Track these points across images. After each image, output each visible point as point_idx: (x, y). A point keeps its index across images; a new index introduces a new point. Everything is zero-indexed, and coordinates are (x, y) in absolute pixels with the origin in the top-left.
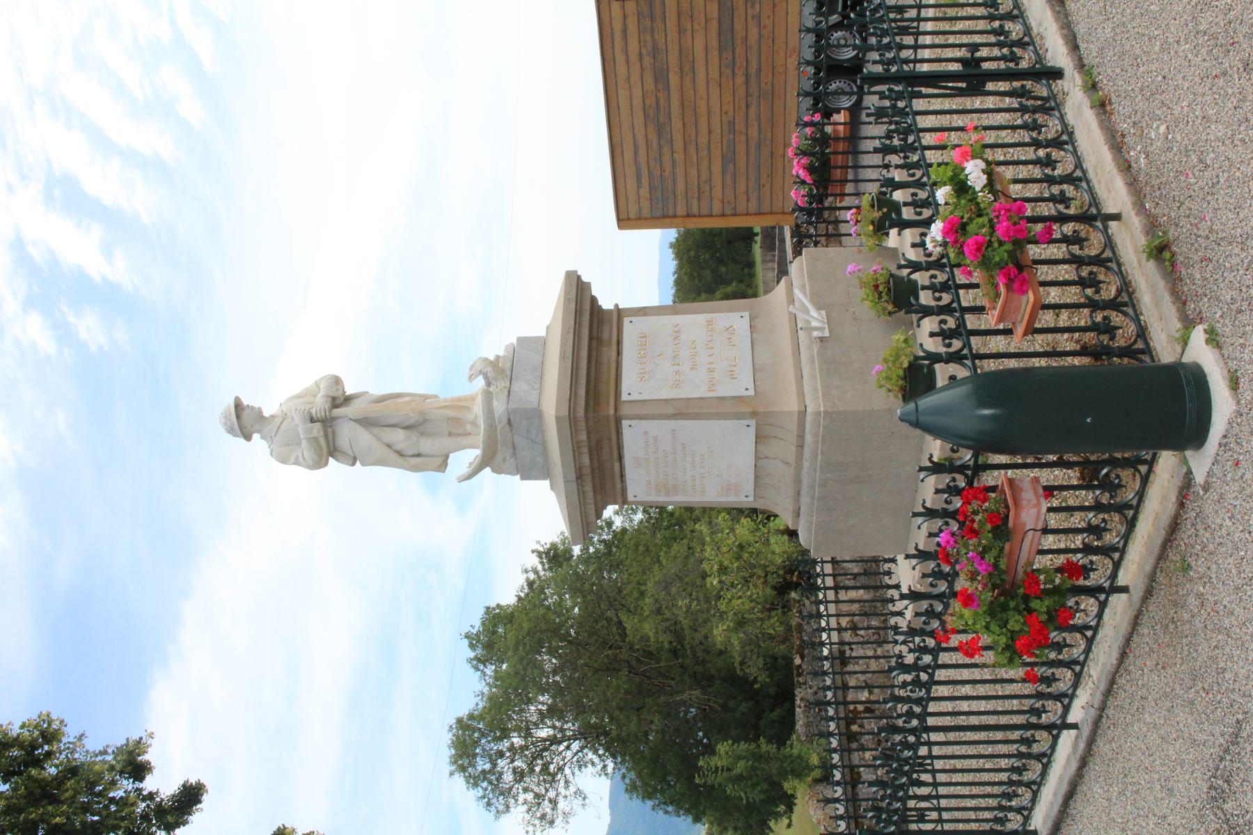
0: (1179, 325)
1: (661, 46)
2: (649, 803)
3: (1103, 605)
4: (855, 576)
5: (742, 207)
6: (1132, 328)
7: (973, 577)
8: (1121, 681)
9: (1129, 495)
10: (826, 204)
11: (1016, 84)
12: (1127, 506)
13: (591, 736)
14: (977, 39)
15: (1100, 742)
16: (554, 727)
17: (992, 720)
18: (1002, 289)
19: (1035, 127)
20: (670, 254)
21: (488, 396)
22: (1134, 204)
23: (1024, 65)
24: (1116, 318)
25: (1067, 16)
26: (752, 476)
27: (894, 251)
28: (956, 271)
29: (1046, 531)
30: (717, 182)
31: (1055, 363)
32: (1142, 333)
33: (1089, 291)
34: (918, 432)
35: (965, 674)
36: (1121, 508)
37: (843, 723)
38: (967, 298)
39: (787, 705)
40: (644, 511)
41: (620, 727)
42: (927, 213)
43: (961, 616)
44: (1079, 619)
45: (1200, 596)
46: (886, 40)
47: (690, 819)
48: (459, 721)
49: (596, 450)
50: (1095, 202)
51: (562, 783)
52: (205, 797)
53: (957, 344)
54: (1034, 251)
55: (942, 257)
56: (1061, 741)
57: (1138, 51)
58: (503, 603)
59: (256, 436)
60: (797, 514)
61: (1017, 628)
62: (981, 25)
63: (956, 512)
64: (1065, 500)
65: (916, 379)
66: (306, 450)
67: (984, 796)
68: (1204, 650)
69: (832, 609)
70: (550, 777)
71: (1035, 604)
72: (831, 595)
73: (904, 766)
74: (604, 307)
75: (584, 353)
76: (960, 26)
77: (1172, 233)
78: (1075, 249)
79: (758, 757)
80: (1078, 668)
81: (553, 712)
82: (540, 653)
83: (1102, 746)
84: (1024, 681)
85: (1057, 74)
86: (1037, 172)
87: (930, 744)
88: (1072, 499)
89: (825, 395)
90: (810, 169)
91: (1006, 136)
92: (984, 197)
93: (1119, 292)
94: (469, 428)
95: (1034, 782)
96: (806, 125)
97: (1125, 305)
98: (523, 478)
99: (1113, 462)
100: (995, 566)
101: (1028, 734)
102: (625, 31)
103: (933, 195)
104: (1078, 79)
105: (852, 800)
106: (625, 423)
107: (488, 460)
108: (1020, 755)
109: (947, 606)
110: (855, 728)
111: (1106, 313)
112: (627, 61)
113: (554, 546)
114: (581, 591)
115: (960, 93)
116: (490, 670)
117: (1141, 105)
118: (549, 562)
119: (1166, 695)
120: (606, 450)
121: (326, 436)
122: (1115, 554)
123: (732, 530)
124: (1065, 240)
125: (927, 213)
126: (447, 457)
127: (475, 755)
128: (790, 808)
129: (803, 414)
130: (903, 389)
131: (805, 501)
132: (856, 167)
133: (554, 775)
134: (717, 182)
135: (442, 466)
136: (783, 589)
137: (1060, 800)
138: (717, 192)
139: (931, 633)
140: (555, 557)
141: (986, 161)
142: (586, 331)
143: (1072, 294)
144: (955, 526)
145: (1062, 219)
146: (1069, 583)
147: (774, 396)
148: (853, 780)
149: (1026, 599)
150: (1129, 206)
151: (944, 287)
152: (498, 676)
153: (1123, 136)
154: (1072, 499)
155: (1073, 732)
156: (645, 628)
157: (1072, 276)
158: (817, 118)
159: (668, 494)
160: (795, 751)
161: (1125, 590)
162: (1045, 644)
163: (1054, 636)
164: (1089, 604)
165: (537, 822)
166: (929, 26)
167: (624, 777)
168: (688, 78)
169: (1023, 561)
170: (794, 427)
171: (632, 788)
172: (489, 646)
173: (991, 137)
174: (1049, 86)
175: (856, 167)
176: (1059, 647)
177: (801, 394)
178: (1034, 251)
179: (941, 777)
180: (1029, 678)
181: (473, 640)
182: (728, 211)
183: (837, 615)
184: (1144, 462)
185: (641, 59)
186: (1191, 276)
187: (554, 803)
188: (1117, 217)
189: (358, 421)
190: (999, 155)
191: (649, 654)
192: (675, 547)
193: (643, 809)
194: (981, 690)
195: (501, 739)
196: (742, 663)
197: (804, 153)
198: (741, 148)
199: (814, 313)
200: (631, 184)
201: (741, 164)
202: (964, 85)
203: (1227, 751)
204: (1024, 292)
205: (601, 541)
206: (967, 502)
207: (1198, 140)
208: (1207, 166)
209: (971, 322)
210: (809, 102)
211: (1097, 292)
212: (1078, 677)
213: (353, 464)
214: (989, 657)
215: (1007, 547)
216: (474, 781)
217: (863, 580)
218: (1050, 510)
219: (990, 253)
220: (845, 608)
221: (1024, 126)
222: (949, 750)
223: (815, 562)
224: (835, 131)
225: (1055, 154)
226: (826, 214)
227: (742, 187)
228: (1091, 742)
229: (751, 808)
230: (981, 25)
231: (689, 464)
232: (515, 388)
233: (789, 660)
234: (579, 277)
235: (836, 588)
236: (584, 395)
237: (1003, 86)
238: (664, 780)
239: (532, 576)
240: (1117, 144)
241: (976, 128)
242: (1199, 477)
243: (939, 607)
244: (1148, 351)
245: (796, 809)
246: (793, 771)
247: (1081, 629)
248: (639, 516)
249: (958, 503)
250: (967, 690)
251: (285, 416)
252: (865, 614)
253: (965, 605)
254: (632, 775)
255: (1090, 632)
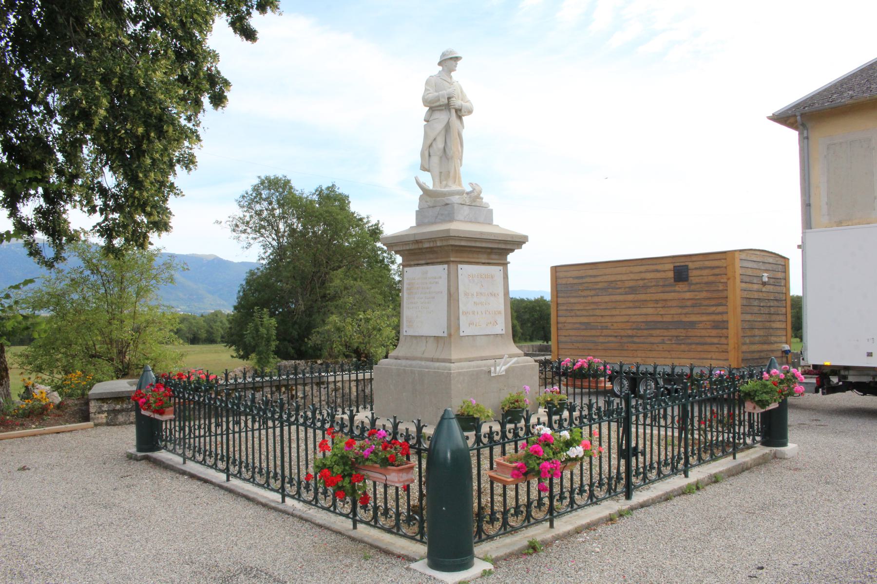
0: (493, 556)
1: (649, 290)
2: (244, 283)
3: (347, 516)
4: (364, 391)
5: (562, 333)
6: (492, 533)
7: (362, 448)
8: (307, 525)
9: (404, 530)
10: (562, 378)
11: (623, 475)
12: (399, 529)
13: (280, 251)
14: (648, 456)
15: (275, 514)
16: (285, 232)
17: (287, 459)
18: (514, 465)
19: (601, 485)
20: (538, 296)
21: (461, 193)
22: (558, 535)
23: (634, 480)
24: (498, 525)
25: (659, 502)
26: (416, 334)
27: (536, 412)
28: (525, 441)
29: (386, 487)
30: (574, 320)
31: (475, 493)
32: (490, 538)
33: (512, 511)
34: (439, 419)
35: (311, 446)
36: (397, 525)
37: (285, 383)
38: (510, 448)
39: (296, 356)
40: (400, 281)
41: (285, 267)
42: (556, 426)
43: (341, 442)
44: (339, 504)
45: (351, 565)
46: (648, 407)
47: (236, 304)
48: (289, 181)
49: (432, 250)
50: (560, 515)
51: (255, 236)
52: (249, 42)
53: (485, 440)
54: (534, 482)
55: (532, 434)
56: (276, 494)
57: (639, 538)
58: (351, 205)
59: (440, 68)
60: (397, 358)
61: (335, 470)
62: (655, 458)
63: (396, 439)
64: (402, 498)
65: (469, 422)
66: (433, 95)
67: (247, 454)
68: (322, 566)
69: (346, 377)
70: (258, 230)
71: (347, 480)
72: (353, 377)
73: (263, 413)
74: (509, 256)
75: (484, 245)
76: (655, 447)
77: (542, 554)
78: (535, 504)
79: (268, 340)
80: (314, 503)
81: (293, 231)
82: (324, 224)
83: (273, 515)
84: (307, 473)
85: (628, 496)
86: (576, 485)
87: (274, 427)
88: (403, 501)
89: (460, 373)
90: (581, 368)
91: (596, 470)
92: (563, 456)
93: (511, 526)
94: (444, 183)
95: (254, 480)
96: (605, 366)
97: (505, 529)
98: (417, 211)
99: (422, 521)
100: (367, 459)
101: (279, 477)
102: (657, 271)
103: (566, 429)
104: (625, 507)
105: (245, 388)
106: (446, 266)
107: (426, 192)
108: (268, 473)
109: (346, 434)
110: (283, 389)
111: (501, 520)
112: (641, 272)
113: (381, 232)
114: (358, 246)
115: (620, 446)
116: (316, 198)
117: (610, 539)
118: (373, 230)
119: (300, 547)
120: (431, 256)
121: (440, 106)
122: (374, 523)
123: (388, 326)
124: (540, 499)
125: (556, 426)
126: (429, 171)
127: (269, 189)
128: (242, 357)
129: (450, 361)
130: (463, 414)
131: (404, 362)
132: (582, 394)
133: (259, 232)
134: (574, 320)
135: (424, 168)
136: (357, 352)
137: (245, 493)
138: (570, 320)
139: (331, 427)
140: (375, 232)
141: (582, 458)
142: (495, 246)
143: (511, 503)
144: (388, 438)
145: (551, 498)
146: (358, 498)
147: (459, 346)
148: (256, 388)
149: (350, 475)
150: (557, 533)
151: (516, 435)
152: (312, 202)
153: (595, 530)
154: (403, 501)
155: (280, 500)
156: (337, 280)
157: (521, 502)
158: (608, 372)
159: (408, 289)
160: (271, 360)
161: (355, 527)
162: (327, 484)
163: (331, 490)
164: (347, 509)
165: (234, 223)
166: (655, 432)
167: (258, 269)
168: (631, 305)
169: (370, 473)
170: (442, 357)
171: (252, 273)
172: (328, 197)
173: (595, 462)
174: (622, 492)
175: (582, 394)
176: (325, 493)
177: (460, 360)
178: (534, 482)
179: (256, 433)
180: (308, 476)
181: (331, 188)
182: (560, 325)
183: (343, 381)
184: (422, 538)
185: (641, 279)
186: (519, 563)
187: (245, 231)
188: (552, 526)
189: (448, 123)
190: (586, 466)
191: (323, 283)
192: (380, 297)
193: (241, 279)
194: (302, 454)
195: (278, 203)
196: (318, 332)
197: (590, 365)
198: (593, 333)
199: (504, 368)
200: (576, 274)
201: (583, 333)
202: (624, 447)
203: (270, 576)
204: (512, 476)
205: (384, 257)
206: (401, 445)
207: (591, 567)
208: (577, 572)
209: (497, 450)
210: (617, 368)
211: (512, 515)
212: (309, 503)
213: (425, 120)
214: (320, 455)
215: (378, 465)
216: (256, 189)
217: (361, 394)
218: (397, 488)
219: (533, 458)
220: (347, 385)
221: (601, 479)
222: (271, 437)
223: (371, 368)
224: (601, 382)
225: (586, 495)
226: (557, 378)
227: (572, 333)
228: (275, 509)
229: (242, 336)
230: (655, 458)
231: (424, 295)
232: (466, 208)
233: (319, 357)
234: (524, 243)
235: (357, 381)
236: (459, 245)
237: (623, 469)
238: (256, 290)
239: (365, 221)
240: (590, 527)
241: (600, 452)
242: (413, 565)
243: (346, 430)
244: (481, 540)
245: (241, 360)
246: (261, 358)
247: (334, 504)
248: (397, 278)
249: (401, 440)
250: (302, 446)
251: (451, 84)
252: (343, 396)
253: (347, 443)
254: (259, 274)
255: (332, 509)
